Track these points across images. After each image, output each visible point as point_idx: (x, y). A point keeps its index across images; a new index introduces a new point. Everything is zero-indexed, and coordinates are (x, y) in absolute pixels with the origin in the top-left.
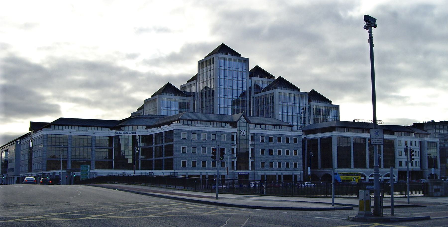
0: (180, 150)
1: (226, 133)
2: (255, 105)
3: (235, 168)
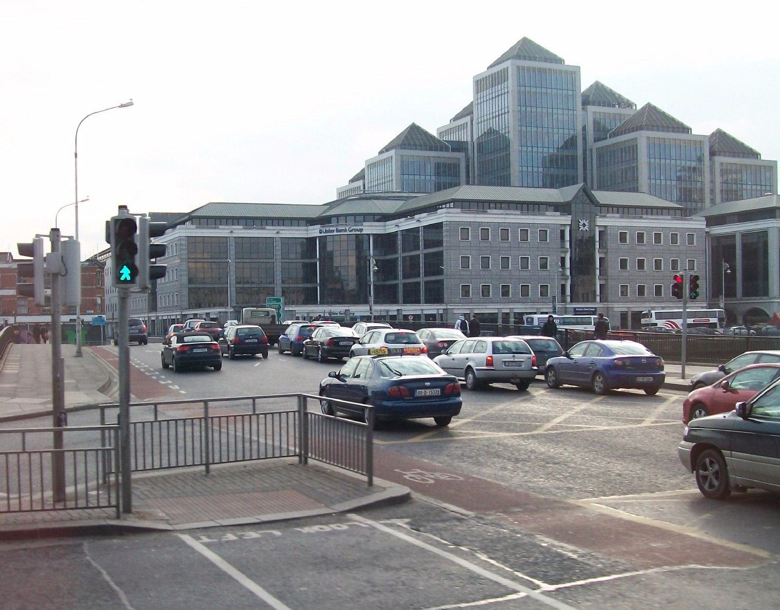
2: (595, 166)
3: (569, 299)
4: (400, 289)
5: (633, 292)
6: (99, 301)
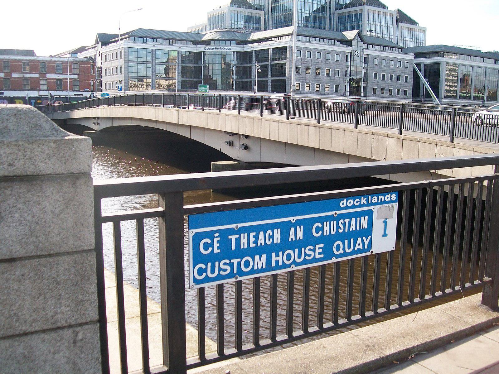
1: (340, 52)
2: (270, 23)
4: (269, 84)
5: (379, 92)
6: (92, 84)
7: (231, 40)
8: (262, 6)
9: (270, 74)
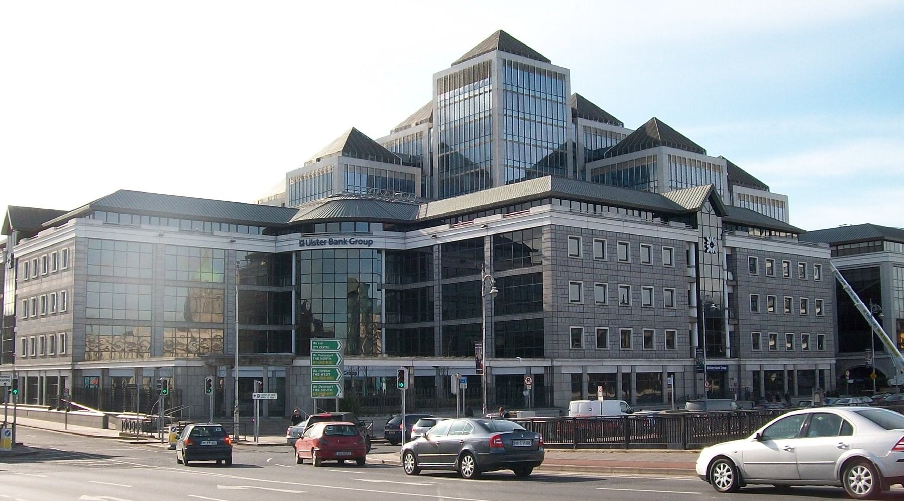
0: (566, 293)
1: (674, 242)
7: (369, 221)
8: (414, 157)
9: (438, 311)
